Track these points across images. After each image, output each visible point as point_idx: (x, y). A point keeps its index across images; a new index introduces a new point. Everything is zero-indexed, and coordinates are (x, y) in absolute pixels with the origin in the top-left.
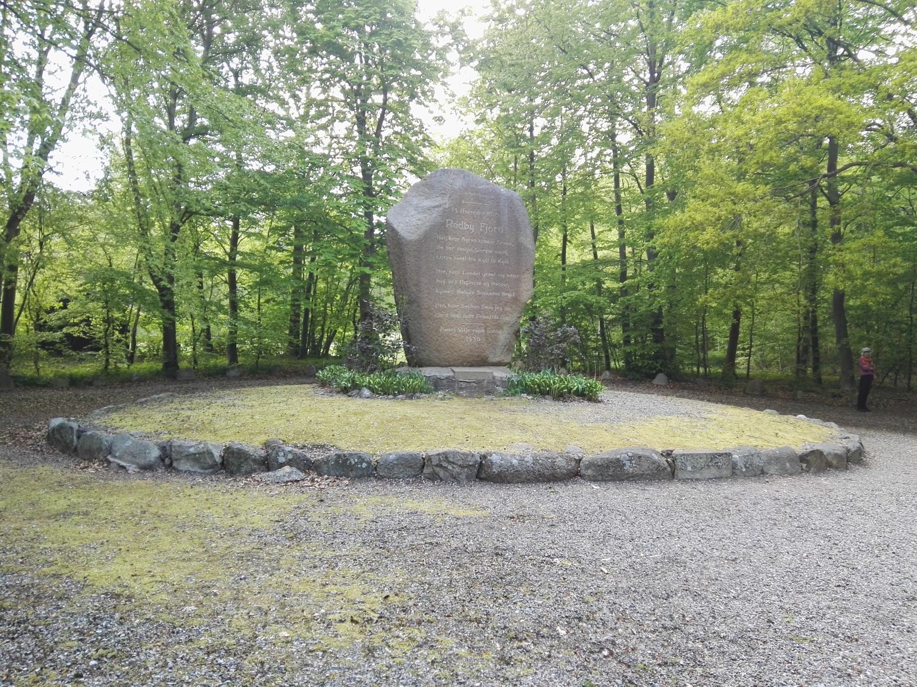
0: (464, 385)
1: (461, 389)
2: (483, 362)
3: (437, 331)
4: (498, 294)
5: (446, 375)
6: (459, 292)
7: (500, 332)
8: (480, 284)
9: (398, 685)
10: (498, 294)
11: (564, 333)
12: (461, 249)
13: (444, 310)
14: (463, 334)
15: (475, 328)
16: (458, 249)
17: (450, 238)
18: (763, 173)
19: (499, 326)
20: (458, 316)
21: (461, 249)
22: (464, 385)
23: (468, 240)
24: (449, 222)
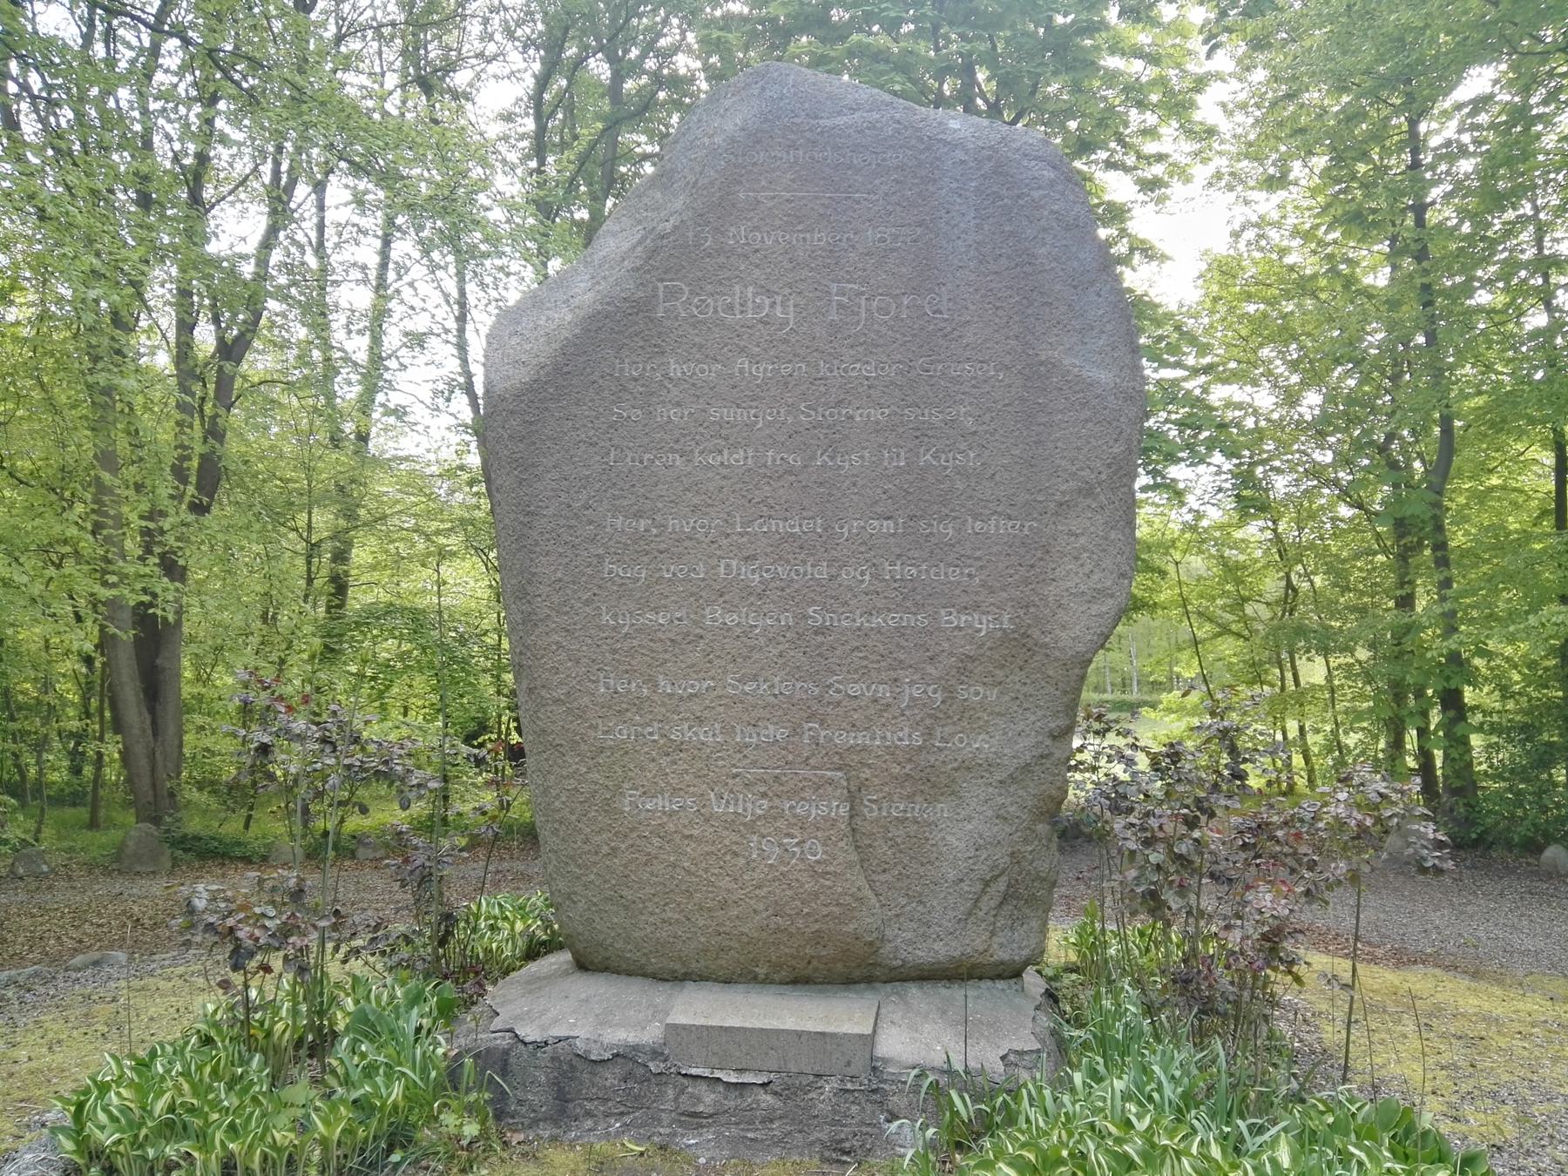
0: (709, 1099)
1: (693, 1120)
2: (860, 970)
3: (608, 808)
4: (921, 620)
5: (620, 1036)
6: (715, 615)
7: (943, 809)
8: (823, 573)
9: (1556, 262)
10: (921, 620)
11: (1278, 720)
12: (729, 414)
13: (639, 704)
14: (731, 824)
15: (795, 793)
16: (715, 414)
17: (675, 369)
18: (906, 1003)
19: (930, 781)
20: (707, 735)
21: (729, 414)
22: (709, 1099)
23: (764, 370)
24: (672, 294)
